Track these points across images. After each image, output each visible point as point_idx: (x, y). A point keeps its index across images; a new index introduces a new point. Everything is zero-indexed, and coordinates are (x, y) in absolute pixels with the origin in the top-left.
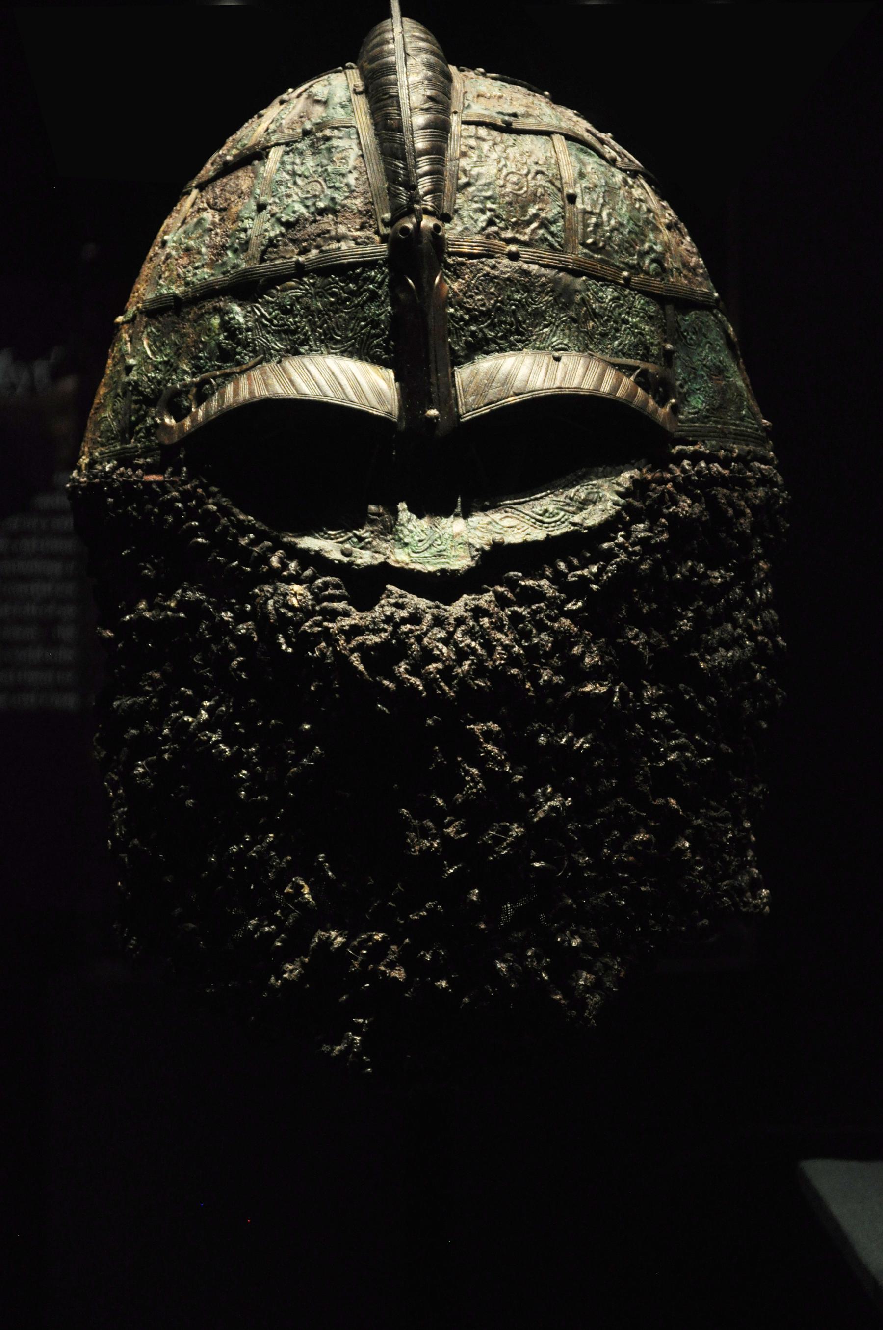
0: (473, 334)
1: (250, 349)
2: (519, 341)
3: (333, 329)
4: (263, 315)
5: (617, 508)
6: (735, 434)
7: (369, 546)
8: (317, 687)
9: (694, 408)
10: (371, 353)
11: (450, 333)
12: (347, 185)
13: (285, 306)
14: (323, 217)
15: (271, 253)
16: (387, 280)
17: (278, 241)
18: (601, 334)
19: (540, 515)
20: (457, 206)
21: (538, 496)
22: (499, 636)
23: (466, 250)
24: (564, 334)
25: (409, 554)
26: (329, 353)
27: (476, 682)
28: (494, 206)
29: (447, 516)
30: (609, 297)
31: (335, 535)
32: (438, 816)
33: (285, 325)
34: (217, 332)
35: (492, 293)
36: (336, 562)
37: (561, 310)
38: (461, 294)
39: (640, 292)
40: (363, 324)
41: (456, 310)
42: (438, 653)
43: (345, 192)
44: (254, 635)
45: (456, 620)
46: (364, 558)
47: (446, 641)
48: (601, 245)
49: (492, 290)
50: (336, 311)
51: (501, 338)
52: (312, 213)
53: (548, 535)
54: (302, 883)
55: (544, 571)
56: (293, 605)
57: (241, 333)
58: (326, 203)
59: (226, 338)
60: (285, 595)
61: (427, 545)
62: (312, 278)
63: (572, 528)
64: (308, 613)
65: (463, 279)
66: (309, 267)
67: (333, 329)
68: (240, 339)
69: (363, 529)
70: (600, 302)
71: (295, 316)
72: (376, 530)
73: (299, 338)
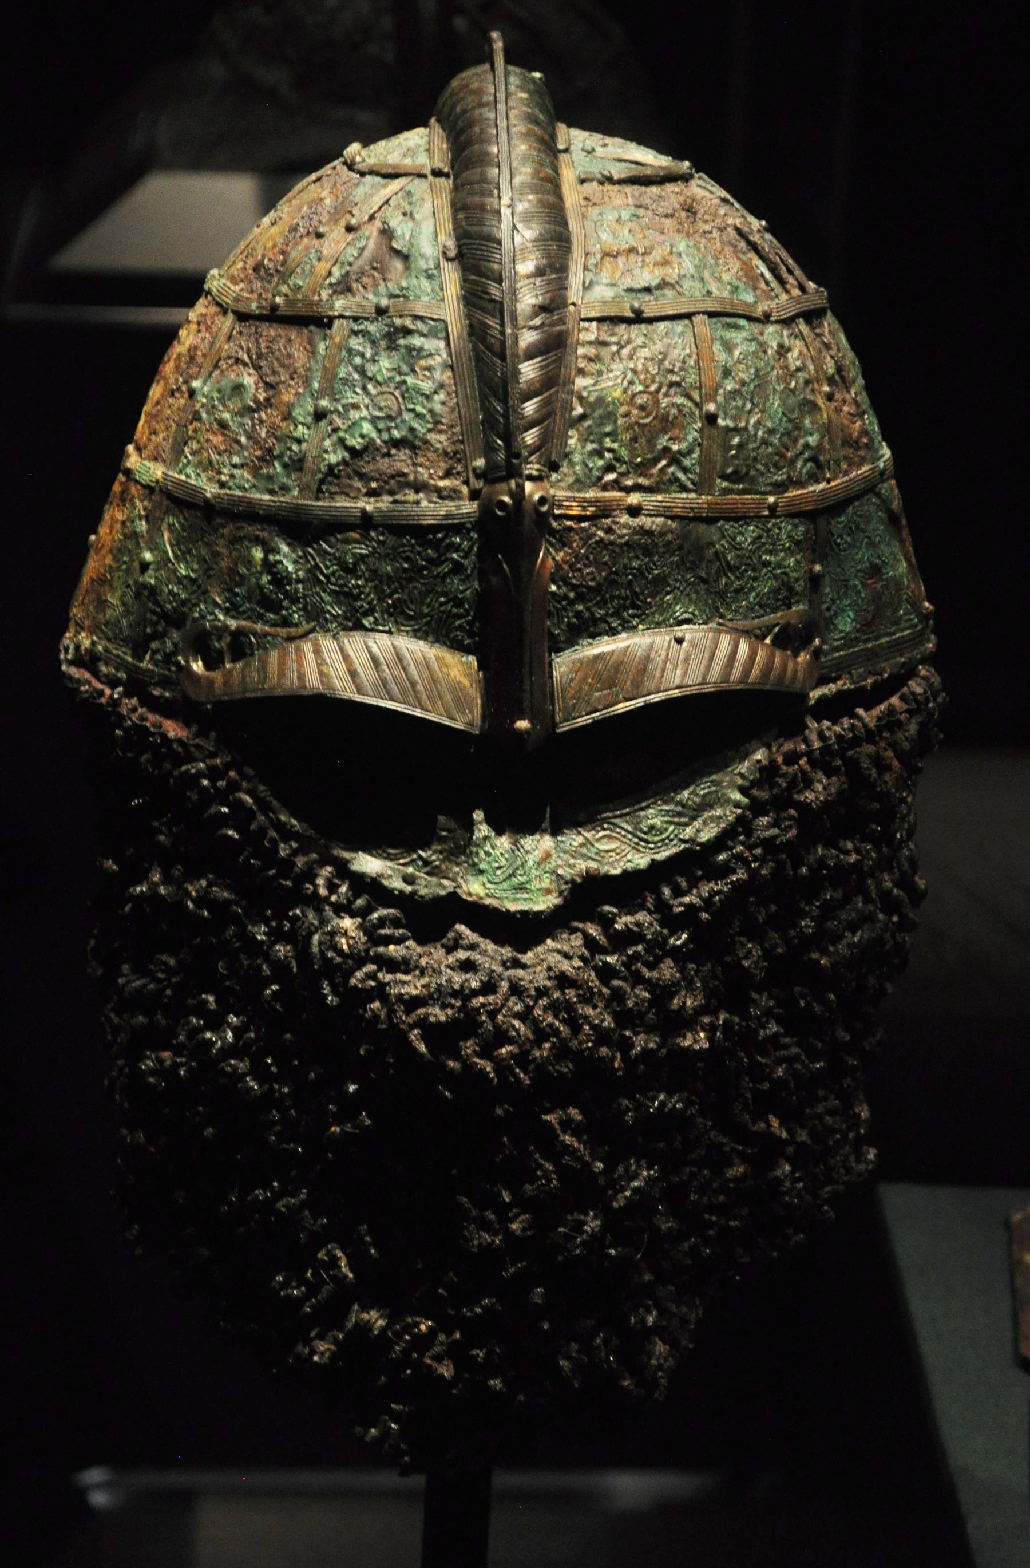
0: (578, 614)
1: (301, 606)
2: (633, 616)
3: (405, 602)
4: (317, 567)
5: (739, 811)
6: (889, 648)
7: (436, 871)
8: (367, 1051)
9: (842, 632)
10: (452, 635)
11: (550, 615)
12: (431, 411)
13: (346, 563)
14: (399, 450)
15: (330, 484)
16: (475, 549)
17: (340, 471)
18: (737, 591)
19: (645, 833)
20: (568, 449)
21: (644, 804)
22: (590, 1011)
23: (574, 512)
24: (690, 600)
25: (484, 885)
26: (399, 631)
27: (558, 1067)
28: (615, 446)
29: (532, 833)
30: (749, 540)
31: (396, 855)
32: (504, 1214)
33: (345, 585)
34: (259, 568)
35: (605, 564)
36: (396, 892)
37: (690, 569)
38: (566, 567)
40: (442, 599)
41: (559, 587)
42: (514, 1034)
43: (428, 422)
44: (294, 964)
45: (537, 989)
46: (428, 887)
47: (522, 1017)
49: (606, 558)
50: (410, 580)
51: (612, 615)
52: (385, 442)
53: (653, 860)
54: (340, 1254)
55: (645, 900)
56: (342, 950)
57: (290, 584)
58: (404, 433)
59: (270, 583)
60: (333, 934)
61: (507, 874)
62: (382, 534)
63: (683, 846)
64: (359, 960)
65: (571, 548)
66: (377, 520)
67: (405, 602)
68: (287, 591)
69: (430, 849)
70: (737, 549)
71: (358, 578)
72: (445, 850)
73: (362, 606)
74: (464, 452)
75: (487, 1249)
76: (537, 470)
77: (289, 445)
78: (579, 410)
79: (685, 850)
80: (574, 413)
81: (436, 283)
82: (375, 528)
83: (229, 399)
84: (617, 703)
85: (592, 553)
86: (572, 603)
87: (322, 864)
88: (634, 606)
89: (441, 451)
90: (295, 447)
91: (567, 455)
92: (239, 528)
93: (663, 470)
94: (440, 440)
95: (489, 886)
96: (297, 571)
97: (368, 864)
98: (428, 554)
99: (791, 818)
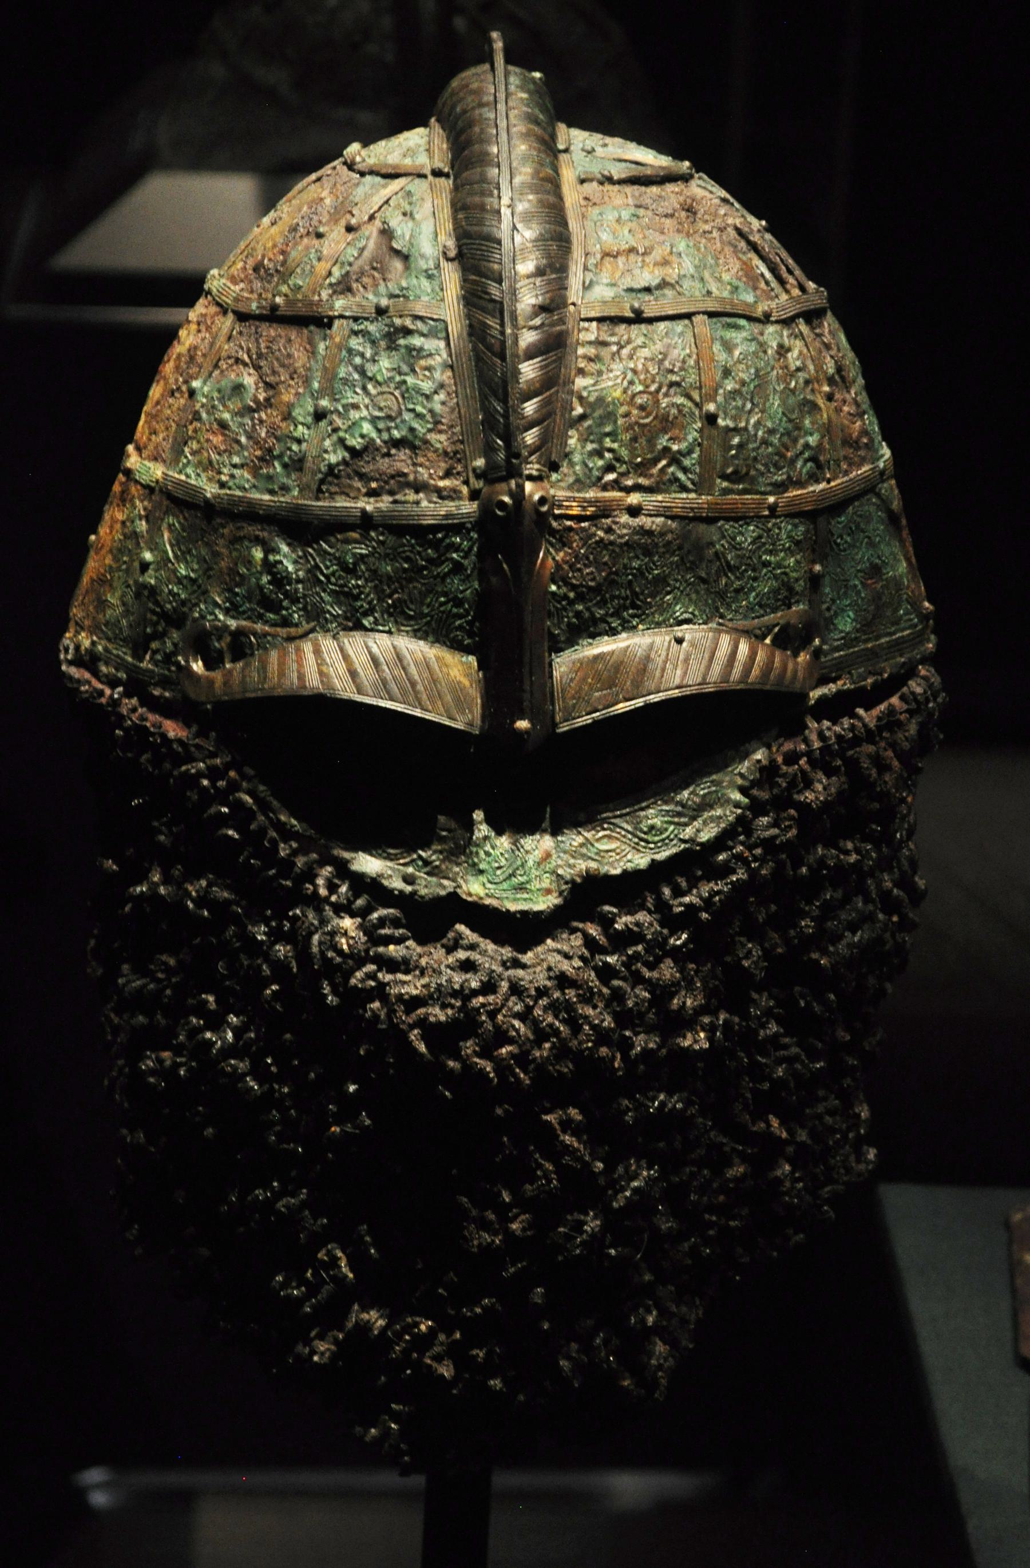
0: (578, 614)
1: (301, 606)
2: (633, 616)
3: (405, 602)
4: (317, 567)
5: (739, 811)
6: (889, 648)
7: (436, 871)
8: (367, 1051)
9: (842, 632)
10: (452, 635)
11: (550, 615)
12: (431, 411)
13: (346, 563)
14: (399, 450)
15: (330, 484)
16: (475, 549)
17: (340, 471)
19: (645, 833)
20: (568, 449)
21: (644, 804)
22: (590, 1011)
23: (574, 512)
24: (690, 600)
25: (484, 885)
26: (399, 631)
27: (558, 1067)
28: (615, 446)
29: (532, 833)
30: (749, 540)
31: (396, 855)
32: (504, 1214)
33: (345, 585)
34: (259, 568)
35: (605, 564)
36: (396, 892)
38: (566, 567)
39: (786, 516)
40: (442, 599)
41: (559, 587)
42: (514, 1034)
43: (428, 422)
44: (294, 964)
46: (428, 887)
47: (522, 1017)
48: (744, 470)
49: (606, 558)
51: (612, 615)
52: (385, 442)
53: (653, 860)
54: (340, 1254)
55: (645, 900)
56: (342, 950)
57: (290, 584)
58: (404, 433)
59: (270, 583)
60: (333, 934)
61: (507, 874)
62: (382, 534)
63: (683, 846)
64: (359, 960)
65: (571, 548)
66: (377, 520)
67: (405, 602)
68: (287, 591)
69: (430, 849)
70: (737, 549)
71: (358, 578)
72: (445, 850)
73: (362, 606)
74: (464, 452)
75: (487, 1249)
77: (289, 445)
78: (579, 410)
79: (685, 850)
80: (574, 413)
81: (436, 283)
82: (375, 528)
83: (229, 399)
84: (617, 703)
85: (592, 553)
86: (572, 603)
87: (322, 864)
88: (634, 606)
90: (295, 447)
91: (567, 455)
92: (239, 528)
93: (663, 470)
95: (489, 886)
96: (297, 571)
97: (368, 864)
98: (428, 554)
99: (791, 818)
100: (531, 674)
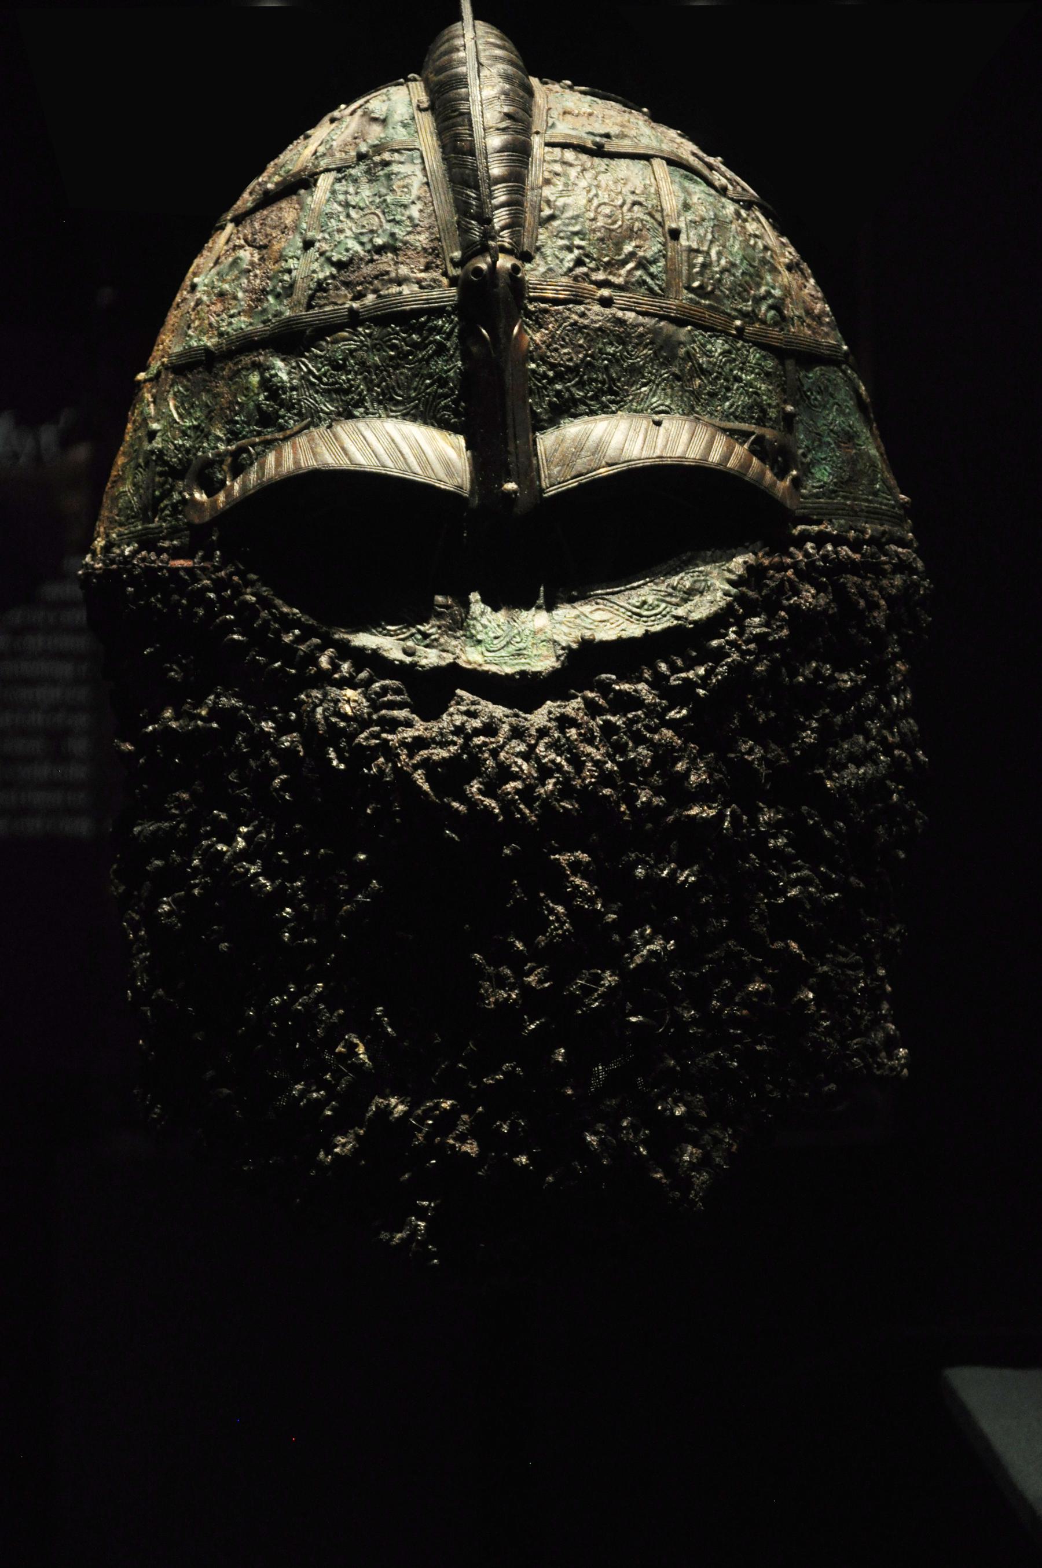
0: (558, 393)
1: (295, 411)
2: (613, 402)
3: (393, 388)
4: (310, 372)
5: (729, 599)
6: (867, 512)
7: (435, 644)
8: (374, 810)
9: (819, 481)
10: (438, 416)
11: (531, 393)
12: (410, 218)
13: (336, 361)
14: (382, 255)
15: (319, 298)
16: (456, 331)
17: (328, 284)
19: (638, 607)
20: (539, 243)
21: (635, 584)
22: (589, 749)
23: (550, 294)
24: (666, 394)
25: (482, 654)
26: (388, 416)
27: (562, 804)
28: (583, 243)
29: (528, 609)
30: (719, 351)
31: (395, 631)
32: (517, 962)
33: (337, 383)
34: (256, 391)
35: (581, 346)
36: (397, 663)
38: (544, 346)
39: (755, 344)
40: (428, 381)
41: (538, 366)
42: (517, 769)
43: (408, 226)
44: (300, 748)
45: (538, 730)
46: (430, 658)
47: (526, 756)
49: (581, 342)
51: (591, 398)
52: (369, 252)
53: (647, 631)
54: (356, 1041)
55: (642, 673)
56: (346, 714)
57: (284, 393)
58: (385, 240)
59: (267, 398)
60: (336, 701)
61: (504, 643)
62: (369, 328)
63: (675, 622)
64: (364, 723)
65: (547, 329)
66: (364, 315)
67: (393, 388)
68: (283, 399)
69: (428, 623)
70: (708, 356)
71: (348, 373)
72: (444, 625)
73: (353, 398)
74: (442, 247)
76: (509, 243)
81: (412, 129)
86: (552, 381)
89: (420, 249)
93: (630, 272)
94: (422, 239)
100: (515, 438)
